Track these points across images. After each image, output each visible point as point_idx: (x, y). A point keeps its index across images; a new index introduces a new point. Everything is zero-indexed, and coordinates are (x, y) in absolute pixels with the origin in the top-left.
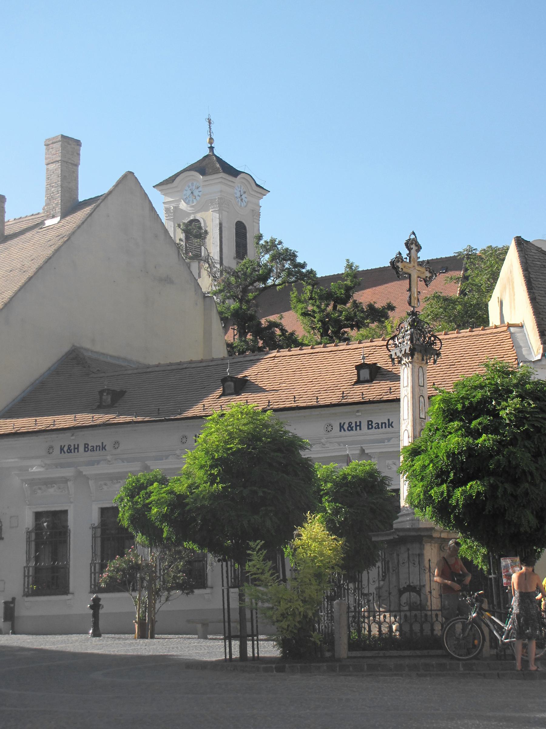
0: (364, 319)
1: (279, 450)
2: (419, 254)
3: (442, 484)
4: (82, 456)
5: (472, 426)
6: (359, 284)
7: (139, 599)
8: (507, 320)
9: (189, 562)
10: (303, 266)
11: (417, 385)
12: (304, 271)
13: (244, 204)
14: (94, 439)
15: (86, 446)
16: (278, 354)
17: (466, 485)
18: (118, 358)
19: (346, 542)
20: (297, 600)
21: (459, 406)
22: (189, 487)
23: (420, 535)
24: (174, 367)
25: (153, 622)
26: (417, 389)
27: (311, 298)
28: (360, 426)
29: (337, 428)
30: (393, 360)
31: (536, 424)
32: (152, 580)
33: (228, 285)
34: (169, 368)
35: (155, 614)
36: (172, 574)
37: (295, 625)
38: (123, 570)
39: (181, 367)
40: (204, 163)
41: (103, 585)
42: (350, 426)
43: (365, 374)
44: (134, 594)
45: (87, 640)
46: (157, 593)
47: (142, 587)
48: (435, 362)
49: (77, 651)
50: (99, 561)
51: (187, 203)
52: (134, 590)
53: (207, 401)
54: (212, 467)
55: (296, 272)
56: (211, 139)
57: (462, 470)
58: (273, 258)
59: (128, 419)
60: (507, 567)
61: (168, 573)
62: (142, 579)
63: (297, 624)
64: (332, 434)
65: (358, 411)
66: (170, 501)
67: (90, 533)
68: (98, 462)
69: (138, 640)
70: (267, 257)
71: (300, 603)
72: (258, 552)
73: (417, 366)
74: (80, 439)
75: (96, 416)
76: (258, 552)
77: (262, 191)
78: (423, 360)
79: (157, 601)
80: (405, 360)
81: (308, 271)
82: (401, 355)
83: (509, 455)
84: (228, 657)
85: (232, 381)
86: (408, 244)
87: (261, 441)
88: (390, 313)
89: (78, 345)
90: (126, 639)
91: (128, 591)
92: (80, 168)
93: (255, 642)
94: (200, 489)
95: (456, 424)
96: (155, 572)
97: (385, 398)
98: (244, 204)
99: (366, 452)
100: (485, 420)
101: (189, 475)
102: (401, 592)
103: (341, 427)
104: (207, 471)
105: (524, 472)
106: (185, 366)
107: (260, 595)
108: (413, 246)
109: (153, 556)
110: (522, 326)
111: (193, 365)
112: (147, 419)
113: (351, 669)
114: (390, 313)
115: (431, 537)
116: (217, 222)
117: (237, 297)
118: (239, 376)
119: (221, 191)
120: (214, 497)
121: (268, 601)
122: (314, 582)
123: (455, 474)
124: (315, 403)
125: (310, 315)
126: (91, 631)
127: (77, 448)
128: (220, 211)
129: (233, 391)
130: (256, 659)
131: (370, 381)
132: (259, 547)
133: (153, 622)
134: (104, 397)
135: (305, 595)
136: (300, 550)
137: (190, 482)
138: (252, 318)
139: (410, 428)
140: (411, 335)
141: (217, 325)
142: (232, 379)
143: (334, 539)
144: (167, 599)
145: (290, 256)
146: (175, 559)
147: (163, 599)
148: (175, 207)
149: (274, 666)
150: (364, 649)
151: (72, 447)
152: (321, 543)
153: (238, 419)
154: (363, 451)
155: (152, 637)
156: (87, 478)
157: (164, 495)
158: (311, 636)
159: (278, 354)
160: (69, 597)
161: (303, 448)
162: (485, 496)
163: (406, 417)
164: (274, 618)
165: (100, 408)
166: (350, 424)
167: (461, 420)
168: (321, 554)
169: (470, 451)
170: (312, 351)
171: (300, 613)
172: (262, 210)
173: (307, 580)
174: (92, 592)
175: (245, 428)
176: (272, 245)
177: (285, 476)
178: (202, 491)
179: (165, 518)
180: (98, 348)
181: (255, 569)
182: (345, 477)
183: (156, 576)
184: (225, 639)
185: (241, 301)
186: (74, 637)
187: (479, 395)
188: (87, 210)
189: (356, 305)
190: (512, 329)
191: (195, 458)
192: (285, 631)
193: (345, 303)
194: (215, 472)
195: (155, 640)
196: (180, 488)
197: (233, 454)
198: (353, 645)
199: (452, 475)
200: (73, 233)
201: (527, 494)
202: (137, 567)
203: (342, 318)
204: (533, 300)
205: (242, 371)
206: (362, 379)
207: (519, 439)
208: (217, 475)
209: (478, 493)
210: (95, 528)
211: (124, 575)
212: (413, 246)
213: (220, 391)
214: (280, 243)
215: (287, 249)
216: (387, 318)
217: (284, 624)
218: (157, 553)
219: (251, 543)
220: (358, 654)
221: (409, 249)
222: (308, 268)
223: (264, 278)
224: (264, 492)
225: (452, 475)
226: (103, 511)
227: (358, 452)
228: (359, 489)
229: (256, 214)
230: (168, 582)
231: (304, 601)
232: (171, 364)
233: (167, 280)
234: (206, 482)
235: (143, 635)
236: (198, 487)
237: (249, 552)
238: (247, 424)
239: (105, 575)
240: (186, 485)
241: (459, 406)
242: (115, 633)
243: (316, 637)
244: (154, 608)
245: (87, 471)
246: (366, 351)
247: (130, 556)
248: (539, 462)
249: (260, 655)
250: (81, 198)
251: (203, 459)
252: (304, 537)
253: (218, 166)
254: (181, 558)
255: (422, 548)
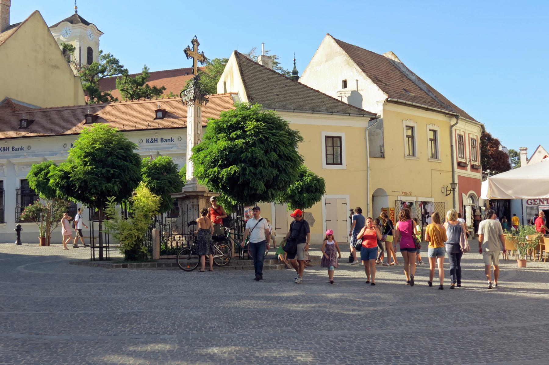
0: (151, 93)
1: (122, 149)
2: (198, 48)
3: (214, 167)
4: (10, 153)
5: (231, 136)
6: (149, 77)
7: (42, 226)
8: (228, 91)
9: (68, 208)
10: (122, 67)
11: (196, 116)
12: (122, 69)
13: (91, 39)
14: (17, 144)
15: (13, 148)
16: (114, 104)
17: (228, 167)
18: (30, 105)
19: (161, 198)
20: (134, 230)
21: (225, 126)
22: (72, 168)
23: (197, 195)
24: (59, 109)
25: (49, 238)
26: (196, 119)
27: (125, 83)
28: (157, 140)
29: (145, 141)
30: (184, 103)
31: (266, 135)
32: (48, 217)
33: (85, 75)
34: (57, 109)
35: (50, 234)
36: (59, 214)
37: (132, 243)
38: (33, 212)
39: (63, 109)
40: (72, 18)
41: (22, 219)
42: (152, 140)
43: (160, 114)
44: (40, 223)
45: (14, 247)
46: (51, 223)
47: (43, 220)
48: (206, 104)
49: (8, 253)
50: (20, 206)
51: (64, 37)
52: (38, 221)
53: (78, 127)
54: (85, 157)
55: (119, 70)
56: (76, 7)
57: (226, 159)
58: (108, 62)
59: (36, 134)
60: (247, 212)
61: (56, 213)
62: (43, 216)
63: (134, 242)
64: (142, 144)
65: (156, 133)
66: (61, 175)
67: (15, 192)
68: (19, 156)
69: (41, 247)
70: (105, 62)
71: (136, 231)
72: (112, 203)
73: (197, 106)
74: (10, 144)
75: (18, 133)
76: (112, 203)
77: (101, 33)
78: (200, 103)
79: (51, 227)
80: (190, 103)
81: (124, 70)
82: (188, 100)
83: (252, 152)
84: (93, 257)
85: (90, 116)
86: (193, 42)
87: (112, 143)
88: (163, 91)
89: (9, 97)
90: (35, 246)
91: (35, 222)
92: (11, 8)
93: (108, 252)
94: (78, 169)
95: (223, 134)
96: (50, 213)
97: (171, 126)
98: (91, 39)
99: (160, 153)
100: (239, 132)
101: (71, 161)
102: (189, 225)
103: (147, 141)
104: (82, 159)
105: (260, 160)
106: (66, 108)
107: (113, 226)
108: (195, 43)
109: (49, 205)
110: (238, 94)
111: (70, 108)
112: (45, 134)
113: (164, 266)
114: (163, 91)
115: (203, 196)
116: (79, 47)
117: (89, 80)
118: (95, 114)
119: (81, 32)
120: (86, 173)
121: (117, 230)
122: (143, 220)
123: (222, 162)
124: (134, 129)
125: (125, 91)
126: (16, 242)
127: (8, 149)
128: (80, 41)
129: (91, 121)
130: (108, 259)
131: (163, 118)
132: (113, 200)
133: (49, 238)
134: (23, 123)
135: (138, 226)
136: (136, 202)
137: (72, 165)
138: (96, 90)
139: (192, 139)
140: (195, 90)
141: (81, 92)
142: (90, 115)
143: (155, 196)
144: (56, 226)
145: (116, 62)
146: (61, 206)
147: (54, 226)
148: (57, 39)
149: (121, 264)
150: (168, 255)
151: (6, 148)
152: (147, 198)
153: (99, 132)
154: (158, 153)
155: (49, 245)
156: (14, 164)
157: (57, 172)
158: (141, 249)
159: (114, 104)
160: (4, 224)
161: (134, 148)
162: (239, 174)
163: (190, 133)
164: (121, 239)
165: (21, 128)
166: (152, 140)
167: (225, 133)
168: (148, 205)
169: (231, 150)
170: (132, 103)
171: (135, 237)
172: (100, 42)
173: (140, 219)
174: (17, 222)
175: (103, 136)
176: (107, 57)
177: (125, 162)
178: (79, 170)
179: (57, 185)
180: (19, 99)
181: (110, 212)
182: (155, 164)
183: (50, 215)
184: (91, 248)
185: (91, 82)
186: (7, 245)
187: (235, 120)
188: (15, 29)
189: (148, 86)
190: (233, 95)
191: (75, 152)
192: (126, 246)
193: (142, 85)
194: (87, 159)
195: (50, 247)
196: (67, 168)
197: (96, 150)
198: (163, 252)
199: (220, 162)
200: (7, 39)
201: (261, 173)
202: (40, 210)
203: (140, 93)
204: (244, 81)
205: (96, 112)
206: (158, 117)
207: (257, 143)
208: (88, 161)
209: (235, 172)
210: (18, 190)
211: (34, 214)
212: (195, 43)
213: (84, 121)
214: (112, 56)
215: (114, 59)
216: (162, 93)
217: (127, 242)
218: (51, 202)
219: (108, 198)
220: (165, 257)
221: (194, 45)
222: (125, 68)
223: (102, 72)
224: (114, 171)
225: (220, 162)
226: (22, 181)
227: (156, 154)
228: (162, 171)
229: (98, 44)
230: (57, 218)
231: (138, 230)
232: (58, 108)
233: (56, 67)
234: (81, 165)
235: (44, 244)
236: (77, 168)
237: (107, 203)
238: (104, 134)
239: (23, 214)
240: (70, 167)
241: (225, 126)
242: (29, 243)
243: (144, 249)
244: (50, 231)
245: (14, 161)
246: (160, 103)
247: (36, 204)
248: (268, 156)
249: (110, 256)
250: (11, 23)
251: (80, 153)
252: (138, 195)
253: (79, 19)
254: (64, 206)
255: (198, 202)
